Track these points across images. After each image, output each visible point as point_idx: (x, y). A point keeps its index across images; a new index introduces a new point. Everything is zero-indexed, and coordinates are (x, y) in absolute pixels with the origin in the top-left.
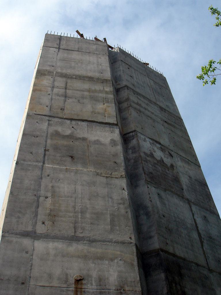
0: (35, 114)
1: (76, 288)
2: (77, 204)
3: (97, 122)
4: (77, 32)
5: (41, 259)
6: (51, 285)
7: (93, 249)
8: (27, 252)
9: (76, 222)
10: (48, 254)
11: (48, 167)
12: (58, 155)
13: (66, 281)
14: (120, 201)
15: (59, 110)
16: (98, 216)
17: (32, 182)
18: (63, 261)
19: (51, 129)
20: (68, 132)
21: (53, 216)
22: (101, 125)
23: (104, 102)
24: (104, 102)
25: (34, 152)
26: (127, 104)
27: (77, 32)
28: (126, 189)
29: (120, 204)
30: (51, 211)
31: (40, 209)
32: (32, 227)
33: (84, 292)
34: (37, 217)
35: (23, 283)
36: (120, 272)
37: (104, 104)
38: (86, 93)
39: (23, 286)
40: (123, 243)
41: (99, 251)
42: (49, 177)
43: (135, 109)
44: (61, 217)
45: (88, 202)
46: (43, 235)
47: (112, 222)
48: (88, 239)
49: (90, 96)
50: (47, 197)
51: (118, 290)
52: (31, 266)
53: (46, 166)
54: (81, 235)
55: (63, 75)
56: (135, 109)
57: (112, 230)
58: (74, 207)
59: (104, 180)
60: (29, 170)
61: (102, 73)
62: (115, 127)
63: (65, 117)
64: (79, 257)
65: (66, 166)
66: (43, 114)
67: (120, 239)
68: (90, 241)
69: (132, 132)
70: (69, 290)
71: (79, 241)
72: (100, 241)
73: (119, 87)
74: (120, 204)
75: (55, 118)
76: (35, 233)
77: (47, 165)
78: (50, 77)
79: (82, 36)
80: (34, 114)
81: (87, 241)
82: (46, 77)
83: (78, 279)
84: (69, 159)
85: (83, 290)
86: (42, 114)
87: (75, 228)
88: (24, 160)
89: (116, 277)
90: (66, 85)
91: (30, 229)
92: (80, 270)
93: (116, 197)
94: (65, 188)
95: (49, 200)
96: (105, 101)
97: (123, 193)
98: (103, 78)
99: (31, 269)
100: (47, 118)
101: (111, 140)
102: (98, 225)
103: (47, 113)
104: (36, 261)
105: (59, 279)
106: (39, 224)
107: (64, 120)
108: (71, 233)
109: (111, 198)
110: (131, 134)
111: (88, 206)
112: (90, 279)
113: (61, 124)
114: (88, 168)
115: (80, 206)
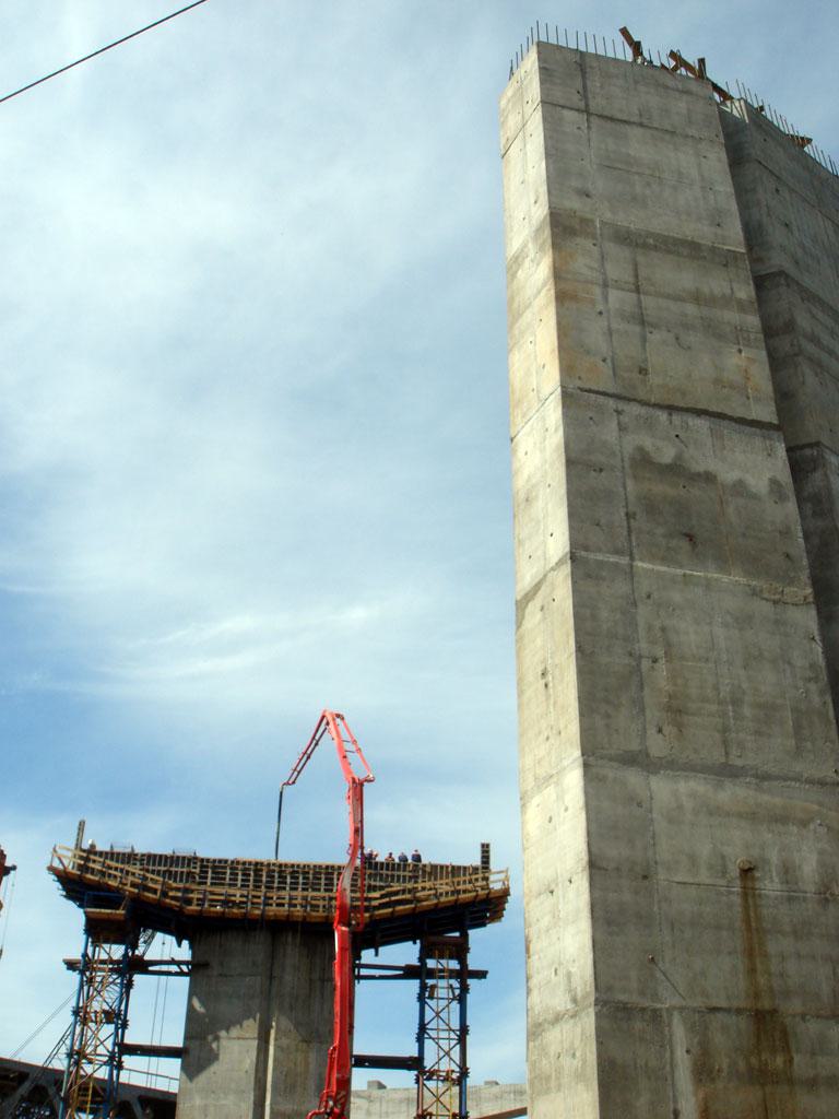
0: (582, 390)
1: (744, 888)
2: (721, 680)
3: (731, 418)
4: (624, 32)
5: (671, 821)
6: (696, 880)
7: (765, 798)
8: (640, 805)
9: (725, 730)
10: (680, 807)
11: (643, 569)
12: (660, 531)
13: (724, 873)
14: (809, 674)
15: (636, 375)
16: (768, 711)
17: (618, 616)
18: (711, 826)
19: (631, 442)
20: (667, 455)
21: (676, 710)
22: (743, 427)
23: (739, 343)
24: (739, 343)
25: (603, 521)
26: (792, 345)
27: (624, 32)
28: (817, 638)
29: (810, 680)
30: (670, 697)
31: (647, 691)
32: (639, 741)
33: (760, 895)
34: (644, 715)
35: (645, 877)
36: (821, 853)
37: (740, 351)
38: (691, 309)
39: (646, 883)
40: (822, 783)
41: (778, 801)
42: (650, 602)
43: (810, 359)
44: (693, 714)
45: (742, 672)
46: (664, 761)
47: (798, 728)
48: (753, 772)
49: (702, 318)
50: (655, 661)
51: (820, 893)
52: (653, 838)
53: (637, 567)
54: (739, 763)
55: (625, 238)
56: (810, 359)
57: (798, 751)
58: (716, 688)
59: (766, 608)
60: (604, 579)
61: (719, 225)
62: (775, 435)
63: (653, 400)
64: (740, 815)
65: (681, 567)
66: (601, 390)
67: (818, 774)
68: (756, 776)
69: (811, 445)
70: (733, 893)
71: (736, 776)
72: (777, 778)
73: (764, 270)
74: (810, 680)
75: (632, 403)
76: (648, 755)
77: (640, 564)
78: (588, 243)
79: (636, 47)
80: (579, 388)
81: (753, 776)
82: (578, 240)
83: (746, 867)
84: (685, 545)
85: (757, 892)
86: (595, 388)
87: (725, 743)
88: (586, 549)
89: (814, 864)
90: (636, 276)
91: (635, 746)
92: (747, 847)
93: (799, 662)
94: (689, 634)
95: (662, 669)
96: (739, 337)
97: (811, 649)
98: (726, 247)
99: (654, 845)
100: (611, 403)
101: (770, 479)
102: (770, 736)
103: (610, 388)
104: (660, 825)
105: (711, 867)
106: (652, 731)
107: (651, 410)
108: (717, 756)
109: (789, 663)
110: (808, 452)
111: (745, 686)
112: (767, 868)
113: (649, 425)
114: (730, 575)
115: (727, 685)
